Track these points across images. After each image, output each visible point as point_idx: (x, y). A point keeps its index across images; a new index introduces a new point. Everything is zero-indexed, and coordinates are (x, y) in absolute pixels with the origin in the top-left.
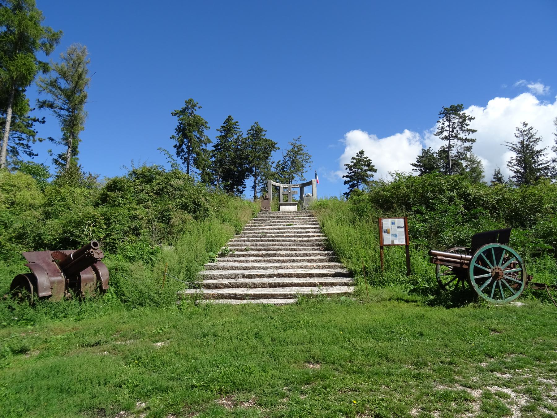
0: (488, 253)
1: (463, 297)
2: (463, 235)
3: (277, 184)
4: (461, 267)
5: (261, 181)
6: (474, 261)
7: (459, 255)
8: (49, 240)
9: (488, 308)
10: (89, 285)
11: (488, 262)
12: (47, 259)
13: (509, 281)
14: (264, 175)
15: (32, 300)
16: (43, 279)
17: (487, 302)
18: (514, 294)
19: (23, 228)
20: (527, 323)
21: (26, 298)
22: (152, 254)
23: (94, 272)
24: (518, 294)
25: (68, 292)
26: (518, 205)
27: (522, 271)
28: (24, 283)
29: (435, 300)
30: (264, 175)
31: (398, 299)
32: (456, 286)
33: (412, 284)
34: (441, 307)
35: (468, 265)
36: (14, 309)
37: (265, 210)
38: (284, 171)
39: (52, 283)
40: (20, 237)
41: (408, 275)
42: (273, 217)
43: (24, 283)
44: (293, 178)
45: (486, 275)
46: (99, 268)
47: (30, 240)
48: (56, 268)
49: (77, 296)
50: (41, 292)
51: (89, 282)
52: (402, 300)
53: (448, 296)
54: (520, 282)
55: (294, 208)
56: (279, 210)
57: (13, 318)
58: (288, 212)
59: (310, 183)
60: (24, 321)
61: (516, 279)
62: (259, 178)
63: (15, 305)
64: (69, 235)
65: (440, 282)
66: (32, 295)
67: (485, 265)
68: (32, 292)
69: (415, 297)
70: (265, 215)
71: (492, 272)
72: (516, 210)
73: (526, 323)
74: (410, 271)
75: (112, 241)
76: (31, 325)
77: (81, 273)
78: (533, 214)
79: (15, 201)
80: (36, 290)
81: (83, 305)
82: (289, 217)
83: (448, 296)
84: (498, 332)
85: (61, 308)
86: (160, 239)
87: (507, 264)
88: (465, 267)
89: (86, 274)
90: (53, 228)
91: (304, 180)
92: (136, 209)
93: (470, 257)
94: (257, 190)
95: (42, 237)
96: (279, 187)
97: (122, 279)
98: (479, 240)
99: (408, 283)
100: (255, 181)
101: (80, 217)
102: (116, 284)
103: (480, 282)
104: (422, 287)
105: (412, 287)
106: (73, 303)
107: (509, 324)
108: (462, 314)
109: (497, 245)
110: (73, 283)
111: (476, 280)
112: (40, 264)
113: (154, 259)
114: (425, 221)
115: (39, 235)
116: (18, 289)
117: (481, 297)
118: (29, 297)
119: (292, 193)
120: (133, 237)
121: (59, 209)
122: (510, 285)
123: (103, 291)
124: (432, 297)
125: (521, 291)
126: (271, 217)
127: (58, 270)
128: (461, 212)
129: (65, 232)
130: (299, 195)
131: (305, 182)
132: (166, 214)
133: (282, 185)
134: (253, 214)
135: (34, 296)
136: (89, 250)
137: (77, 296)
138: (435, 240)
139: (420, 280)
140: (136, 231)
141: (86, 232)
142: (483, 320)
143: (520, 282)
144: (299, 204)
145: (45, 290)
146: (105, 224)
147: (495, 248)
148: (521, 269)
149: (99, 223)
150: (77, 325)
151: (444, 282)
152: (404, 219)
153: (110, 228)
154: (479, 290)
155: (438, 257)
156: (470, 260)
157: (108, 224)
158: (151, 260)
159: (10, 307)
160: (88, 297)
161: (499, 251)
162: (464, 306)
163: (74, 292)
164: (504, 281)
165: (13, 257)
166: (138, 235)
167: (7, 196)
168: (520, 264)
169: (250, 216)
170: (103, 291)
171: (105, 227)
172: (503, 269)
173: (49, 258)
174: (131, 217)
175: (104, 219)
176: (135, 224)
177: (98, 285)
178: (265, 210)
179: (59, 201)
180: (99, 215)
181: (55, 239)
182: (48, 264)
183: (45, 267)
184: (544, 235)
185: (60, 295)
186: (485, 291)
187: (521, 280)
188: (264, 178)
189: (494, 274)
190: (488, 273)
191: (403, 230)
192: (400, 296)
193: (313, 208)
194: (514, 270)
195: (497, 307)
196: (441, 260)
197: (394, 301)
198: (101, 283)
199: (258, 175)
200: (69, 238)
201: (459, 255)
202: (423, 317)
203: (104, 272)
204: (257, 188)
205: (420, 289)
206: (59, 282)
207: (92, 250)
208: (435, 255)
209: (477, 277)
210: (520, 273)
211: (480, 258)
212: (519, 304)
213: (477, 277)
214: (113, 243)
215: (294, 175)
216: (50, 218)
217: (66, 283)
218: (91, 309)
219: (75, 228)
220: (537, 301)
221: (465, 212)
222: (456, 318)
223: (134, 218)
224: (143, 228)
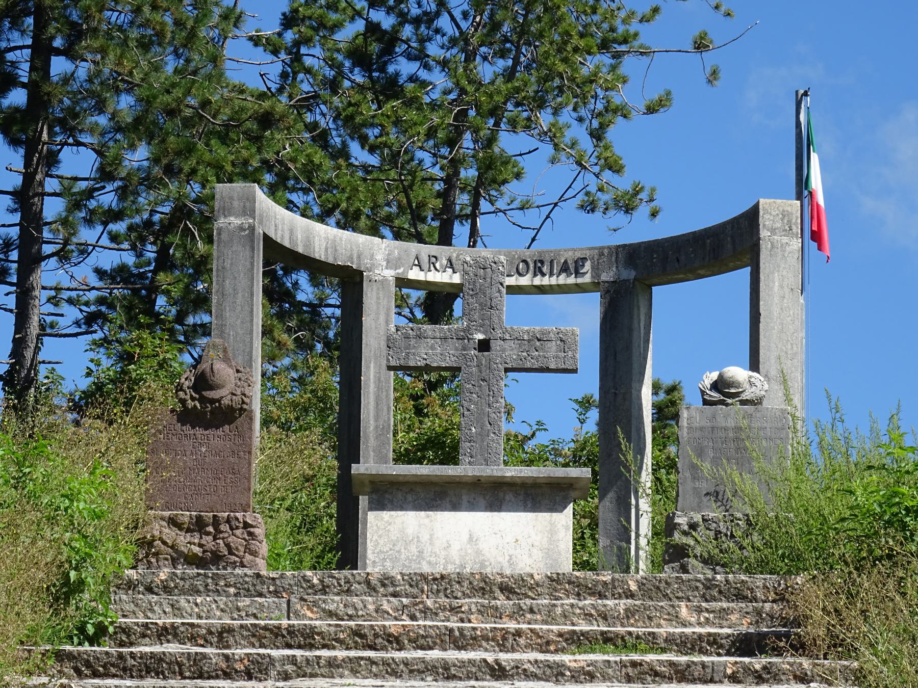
3: (324, 239)
5: (107, 198)
14: (139, 128)
30: (139, 128)
37: (187, 542)
38: (390, 88)
42: (308, 638)
44: (494, 172)
55: (531, 542)
56: (346, 548)
58: (484, 586)
59: (731, 245)
62: (77, 162)
70: (207, 611)
82: (504, 641)
91: (626, 204)
94: (41, 308)
96: (350, 281)
100: (25, 198)
119: (506, 352)
126: (277, 636)
130: (588, 381)
131: (639, 229)
133: (381, 257)
134: (66, 591)
144: (594, 480)
169: (34, 615)
178: (187, 542)
188: (139, 156)
193: (786, 557)
199: (69, 125)
204: (49, 274)
215: (509, 143)
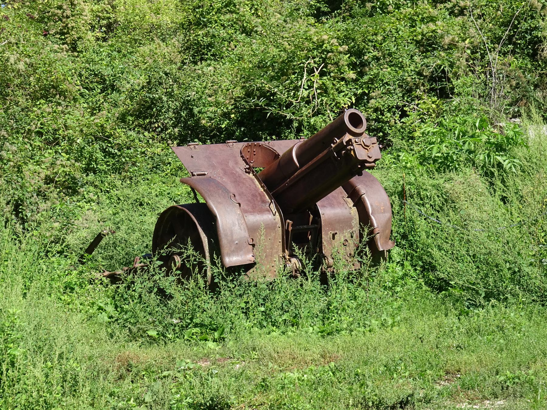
8: (211, 119)
10: (340, 238)
12: (231, 164)
15: (209, 274)
16: (230, 220)
19: (149, 86)
21: (197, 269)
22: (500, 148)
23: (351, 203)
25: (292, 255)
28: (185, 227)
36: (171, 297)
39: (253, 229)
40: (144, 113)
43: (185, 227)
46: (362, 189)
47: (168, 118)
48: (256, 189)
49: (315, 269)
50: (229, 255)
51: (342, 230)
57: (169, 320)
60: (197, 330)
63: (168, 283)
64: (262, 102)
66: (208, 262)
68: (207, 254)
75: (374, 116)
76: (215, 340)
77: (318, 204)
79: (116, 21)
80: (216, 247)
81: (333, 293)
85: (279, 298)
86: (511, 105)
89: (332, 205)
90: (217, 86)
92: (432, 19)
95: (196, 110)
97: (421, 223)
101: (285, 50)
102: (406, 238)
106: (308, 285)
110: (303, 233)
112: (219, 179)
113: (506, 165)
115: (187, 105)
116: (173, 245)
118: (201, 265)
120: (429, 102)
121: (223, 33)
123: (378, 256)
127: (261, 195)
129: (249, 94)
132: (524, 26)
135: (213, 263)
136: (340, 135)
137: (315, 269)
140: (440, 85)
141: (303, 93)
145: (238, 249)
146: (353, 66)
149: (336, 64)
150: (329, 345)
153: (366, 78)
157: (360, 67)
158: (500, 165)
159: (161, 292)
160: (344, 271)
163: (309, 255)
165: (134, 164)
166: (444, 94)
167: (95, 8)
170: (378, 256)
171: (351, 75)
172: (392, 368)
173: (237, 163)
174: (418, 43)
175: (349, 51)
176: (434, 61)
177: (365, 239)
179: (219, 11)
180: (335, 41)
181: (226, 115)
182: (237, 181)
183: (231, 188)
185: (272, 263)
198: (371, 232)
200: (262, 109)
203: (376, 200)
206: (270, 227)
207: (347, 137)
214: (377, 120)
216: (202, 59)
217: (285, 232)
218: (353, 304)
219: (275, 83)
223: (427, 45)
224: (461, 72)
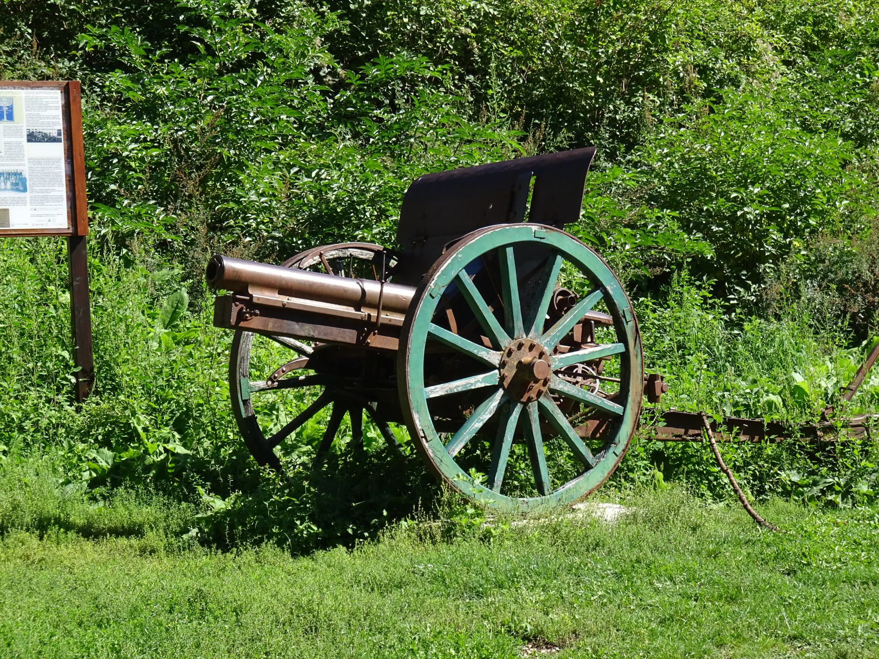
0: (487, 269)
1: (370, 494)
2: (338, 187)
4: (361, 341)
6: (427, 308)
7: (351, 285)
9: (486, 537)
11: (488, 312)
13: (569, 404)
17: (479, 511)
18: (588, 467)
20: (663, 594)
24: (609, 461)
26: (566, 47)
27: (625, 358)
29: (235, 516)
31: (42, 526)
32: (324, 445)
33: (105, 443)
34: (269, 549)
35: (402, 332)
41: (78, 395)
45: (477, 381)
52: (68, 527)
53: (298, 491)
54: (616, 408)
61: (598, 394)
65: (248, 426)
67: (474, 328)
69: (126, 507)
71: (503, 365)
72: (556, 73)
73: (657, 590)
74: (87, 368)
78: (622, 96)
83: (298, 491)
84: (549, 645)
87: (568, 322)
88: (376, 341)
93: (407, 293)
98: (436, 212)
99: (84, 435)
103: (449, 414)
104: (156, 452)
105: (105, 459)
107: (589, 603)
108: (382, 576)
109: (528, 231)
111: (434, 405)
114: (150, 110)
117: (452, 489)
122: (574, 425)
124: (219, 505)
125: (619, 450)
128: (316, 71)
138: (200, 215)
139: (141, 422)
142: (479, 595)
143: (616, 408)
147: (519, 247)
148: (621, 348)
151: (271, 426)
152: (66, 91)
154: (444, 454)
155: (260, 295)
156: (410, 310)
161: (537, 259)
162: (374, 537)
164: (552, 407)
168: (618, 322)
172: (542, 344)
184: (673, 190)
186: (465, 462)
187: (621, 398)
189: (510, 373)
190: (484, 367)
191: (58, 150)
192: (51, 509)
194: (587, 352)
195: (521, 531)
196: (269, 311)
197: (24, 535)
201: (351, 285)
202: (199, 605)
205: (147, 469)
208: (241, 284)
209: (439, 390)
210: (615, 365)
211: (455, 298)
212: (610, 511)
213: (439, 390)
220: (675, 492)
221: (333, 73)
222: (361, 598)
